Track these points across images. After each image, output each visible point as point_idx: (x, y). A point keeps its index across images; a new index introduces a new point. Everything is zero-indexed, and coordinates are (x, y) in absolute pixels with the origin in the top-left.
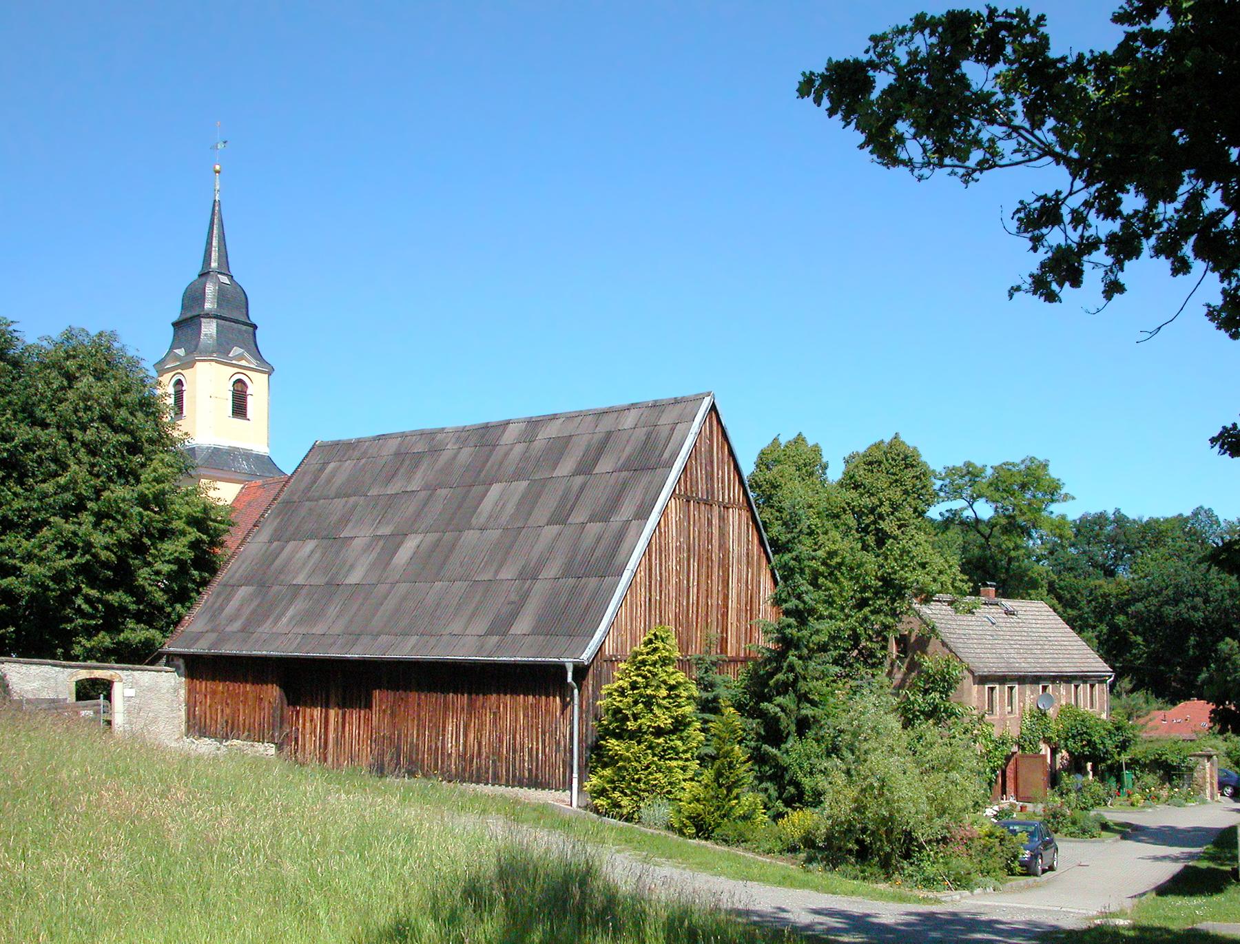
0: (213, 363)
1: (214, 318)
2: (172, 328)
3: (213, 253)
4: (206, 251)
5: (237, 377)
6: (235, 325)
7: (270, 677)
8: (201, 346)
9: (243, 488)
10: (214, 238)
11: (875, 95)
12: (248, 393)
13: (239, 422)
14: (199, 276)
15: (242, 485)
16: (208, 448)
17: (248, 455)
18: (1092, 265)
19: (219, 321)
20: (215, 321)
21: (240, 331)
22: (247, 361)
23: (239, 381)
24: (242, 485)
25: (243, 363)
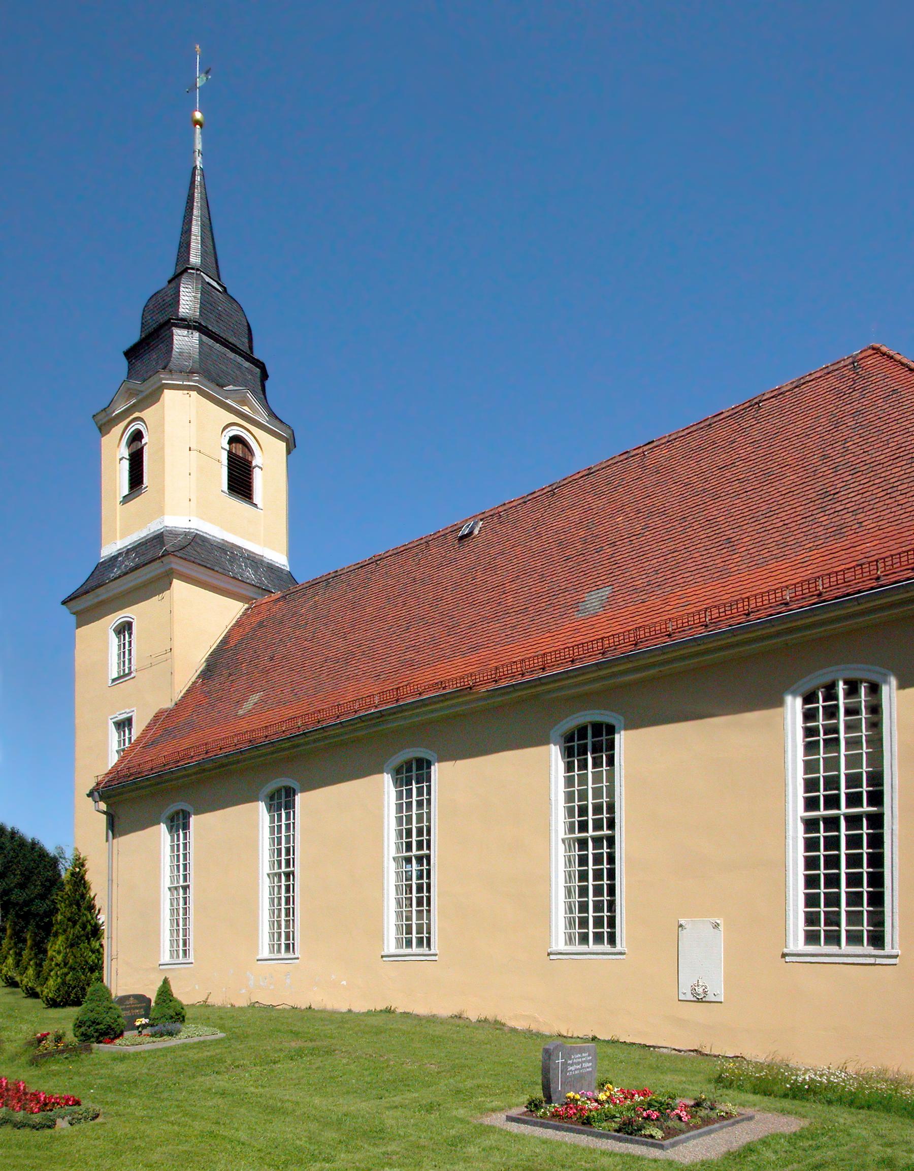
0: (194, 394)
1: (195, 328)
2: (124, 362)
3: (193, 245)
4: (180, 246)
5: (234, 431)
6: (232, 355)
7: (871, 928)
8: (171, 365)
9: (247, 609)
10: (194, 222)
11: (153, 1004)
12: (254, 464)
13: (237, 505)
14: (121, 1034)
15: (247, 606)
16: (186, 534)
17: (255, 561)
18: (710, 998)
19: (204, 338)
20: (196, 334)
21: (240, 367)
22: (251, 407)
23: (234, 440)
24: (247, 606)
25: (246, 409)
